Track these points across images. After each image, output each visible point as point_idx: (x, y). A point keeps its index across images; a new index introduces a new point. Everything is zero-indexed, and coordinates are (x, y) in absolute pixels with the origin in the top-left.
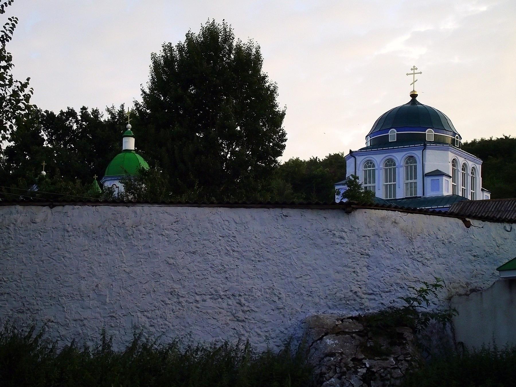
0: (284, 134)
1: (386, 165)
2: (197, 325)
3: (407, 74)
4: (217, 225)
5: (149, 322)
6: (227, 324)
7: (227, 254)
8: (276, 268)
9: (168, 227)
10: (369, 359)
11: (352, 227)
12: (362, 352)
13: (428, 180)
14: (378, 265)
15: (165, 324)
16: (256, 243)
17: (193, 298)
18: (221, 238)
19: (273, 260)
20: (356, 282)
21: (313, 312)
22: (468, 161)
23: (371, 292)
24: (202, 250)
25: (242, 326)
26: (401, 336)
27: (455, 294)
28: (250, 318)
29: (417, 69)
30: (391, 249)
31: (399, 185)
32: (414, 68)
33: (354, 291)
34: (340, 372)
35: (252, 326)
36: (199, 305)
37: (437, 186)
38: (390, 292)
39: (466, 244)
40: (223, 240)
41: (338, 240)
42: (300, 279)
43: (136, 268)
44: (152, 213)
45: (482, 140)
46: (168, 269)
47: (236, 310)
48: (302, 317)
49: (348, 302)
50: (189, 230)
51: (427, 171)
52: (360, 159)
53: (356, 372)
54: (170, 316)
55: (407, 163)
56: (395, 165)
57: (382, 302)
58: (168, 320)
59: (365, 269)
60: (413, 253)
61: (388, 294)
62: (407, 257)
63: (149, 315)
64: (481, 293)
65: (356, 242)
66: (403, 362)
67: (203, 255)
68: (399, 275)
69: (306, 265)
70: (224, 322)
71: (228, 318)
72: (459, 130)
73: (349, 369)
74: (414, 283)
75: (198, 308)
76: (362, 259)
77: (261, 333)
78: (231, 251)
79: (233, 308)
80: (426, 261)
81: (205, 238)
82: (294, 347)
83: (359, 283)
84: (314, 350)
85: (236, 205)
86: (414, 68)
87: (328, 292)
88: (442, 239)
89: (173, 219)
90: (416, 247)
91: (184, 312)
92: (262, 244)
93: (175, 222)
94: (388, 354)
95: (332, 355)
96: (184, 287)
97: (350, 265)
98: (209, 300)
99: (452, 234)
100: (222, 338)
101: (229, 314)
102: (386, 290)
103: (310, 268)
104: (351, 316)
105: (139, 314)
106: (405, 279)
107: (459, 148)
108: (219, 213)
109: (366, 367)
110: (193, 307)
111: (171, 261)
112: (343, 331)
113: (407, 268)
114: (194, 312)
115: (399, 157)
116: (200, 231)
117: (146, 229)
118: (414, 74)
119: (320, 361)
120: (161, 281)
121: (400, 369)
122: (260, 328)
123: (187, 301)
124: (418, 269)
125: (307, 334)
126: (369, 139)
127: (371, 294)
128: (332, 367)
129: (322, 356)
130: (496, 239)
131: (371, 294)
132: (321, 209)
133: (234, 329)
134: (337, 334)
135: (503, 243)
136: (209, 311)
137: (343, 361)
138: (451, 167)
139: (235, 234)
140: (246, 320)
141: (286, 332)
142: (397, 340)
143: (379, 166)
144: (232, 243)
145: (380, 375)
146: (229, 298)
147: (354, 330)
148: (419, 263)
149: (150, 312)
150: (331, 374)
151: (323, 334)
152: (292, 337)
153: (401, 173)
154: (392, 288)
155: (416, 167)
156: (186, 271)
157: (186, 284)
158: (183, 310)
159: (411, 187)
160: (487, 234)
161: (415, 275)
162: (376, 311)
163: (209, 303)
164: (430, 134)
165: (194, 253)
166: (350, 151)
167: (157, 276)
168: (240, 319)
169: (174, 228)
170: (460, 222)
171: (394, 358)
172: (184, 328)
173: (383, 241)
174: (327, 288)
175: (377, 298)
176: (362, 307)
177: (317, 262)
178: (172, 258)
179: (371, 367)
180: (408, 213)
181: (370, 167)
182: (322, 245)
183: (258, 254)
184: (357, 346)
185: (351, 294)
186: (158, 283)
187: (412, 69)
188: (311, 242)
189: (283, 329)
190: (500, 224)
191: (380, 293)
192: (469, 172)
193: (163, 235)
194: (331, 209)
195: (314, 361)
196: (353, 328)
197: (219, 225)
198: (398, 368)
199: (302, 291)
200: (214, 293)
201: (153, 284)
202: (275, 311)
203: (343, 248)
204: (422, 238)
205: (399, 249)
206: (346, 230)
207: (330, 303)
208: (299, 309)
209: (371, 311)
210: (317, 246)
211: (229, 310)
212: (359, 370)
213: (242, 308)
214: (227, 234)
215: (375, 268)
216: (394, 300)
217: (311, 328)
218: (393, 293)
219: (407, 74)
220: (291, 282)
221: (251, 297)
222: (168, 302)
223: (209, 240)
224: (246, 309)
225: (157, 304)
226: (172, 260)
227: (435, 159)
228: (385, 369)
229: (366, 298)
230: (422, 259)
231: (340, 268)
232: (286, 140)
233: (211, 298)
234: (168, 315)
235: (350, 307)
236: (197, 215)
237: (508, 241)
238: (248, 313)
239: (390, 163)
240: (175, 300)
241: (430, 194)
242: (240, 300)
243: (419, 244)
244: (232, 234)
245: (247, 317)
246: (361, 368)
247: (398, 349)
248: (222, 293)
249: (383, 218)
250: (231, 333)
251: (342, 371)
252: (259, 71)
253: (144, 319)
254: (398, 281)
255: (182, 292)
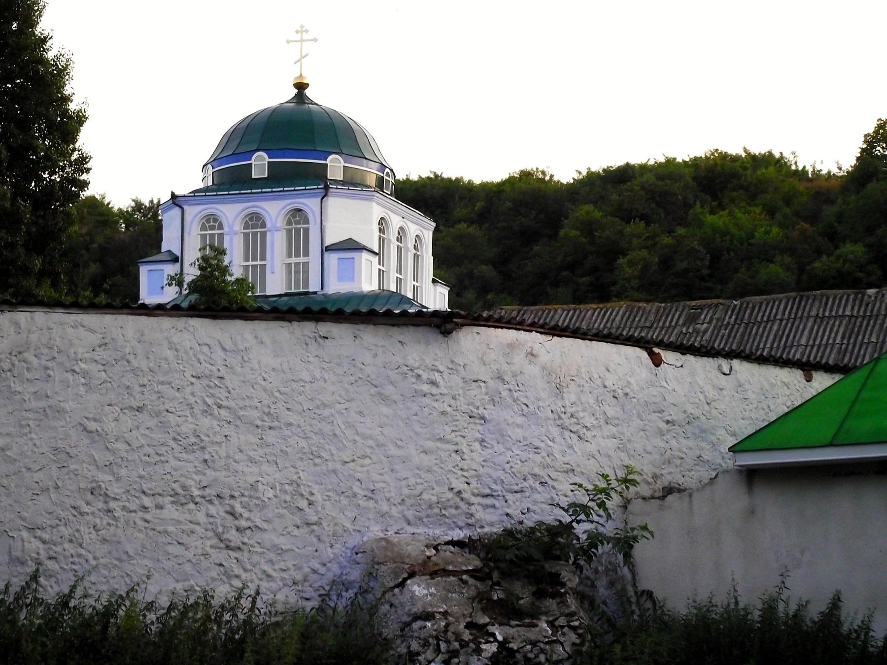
0: (83, 160)
1: (246, 226)
2: (145, 557)
3: (288, 42)
4: (186, 352)
5: (45, 550)
6: (206, 555)
7: (207, 411)
8: (303, 443)
9: (87, 355)
10: (501, 624)
11: (452, 362)
12: (484, 610)
13: (332, 259)
14: (500, 440)
15: (80, 556)
16: (265, 390)
17: (137, 501)
18: (193, 380)
19: (299, 426)
20: (460, 473)
21: (376, 531)
22: (409, 223)
23: (488, 491)
24: (156, 403)
25: (236, 558)
26: (555, 579)
27: (633, 496)
28: (252, 542)
29: (307, 31)
30: (524, 407)
31: (272, 267)
32: (302, 30)
33: (456, 490)
34: (448, 652)
35: (256, 558)
36: (148, 516)
37: (349, 273)
38: (522, 491)
39: (653, 398)
40: (198, 385)
41: (425, 388)
42: (352, 464)
43: (18, 440)
44: (53, 326)
45: (458, 180)
46: (87, 441)
47: (224, 527)
48: (354, 540)
49: (443, 512)
50: (128, 362)
51: (328, 241)
52: (192, 212)
53: (478, 651)
54: (88, 536)
55: (289, 223)
56: (264, 225)
57: (509, 511)
58: (84, 545)
59: (477, 446)
60: (563, 416)
61: (519, 495)
62: (552, 423)
63: (46, 536)
64: (690, 495)
65: (461, 392)
66: (566, 630)
67: (158, 414)
68: (538, 458)
69: (365, 437)
70: (200, 551)
71: (209, 543)
72: (390, 162)
73: (464, 644)
74: (564, 474)
75: (147, 521)
76: (472, 426)
77: (274, 574)
78: (215, 407)
79: (219, 521)
80: (585, 430)
81: (161, 379)
82: (342, 603)
83: (465, 474)
84: (387, 607)
85: (228, 313)
86: (302, 30)
87: (406, 491)
88: (613, 388)
89: (95, 339)
90: (568, 404)
91: (119, 532)
92: (277, 394)
93: (100, 346)
94: (534, 614)
95: (428, 616)
96: (118, 479)
97: (448, 437)
98: (170, 506)
99: (629, 379)
100: (198, 583)
101: (210, 534)
102: (516, 488)
103: (371, 443)
104: (450, 538)
105: (25, 534)
106: (548, 466)
107: (391, 195)
108: (191, 329)
109: (496, 640)
110: (138, 521)
111: (92, 426)
112: (444, 570)
113: (550, 443)
114: (140, 531)
115: (274, 210)
116: (151, 365)
117: (39, 358)
118: (302, 41)
119: (402, 630)
120: (72, 467)
121: (562, 644)
122: (271, 562)
123: (124, 508)
124: (571, 447)
125: (370, 575)
126: (211, 171)
127: (487, 496)
128: (431, 640)
129: (406, 619)
130: (706, 389)
131: (487, 496)
132: (393, 325)
133: (221, 565)
134: (433, 574)
135: (717, 397)
136: (171, 529)
137: (452, 629)
138: (377, 234)
139: (223, 372)
140: (244, 547)
141: (322, 570)
142: (548, 586)
143: (231, 227)
144: (215, 391)
145: (525, 657)
146: (210, 502)
147: (464, 568)
148: (572, 435)
149: (48, 529)
150: (429, 654)
151: (405, 575)
152: (334, 581)
153: (277, 242)
154: (526, 484)
155: (306, 231)
156: (121, 446)
157: (123, 472)
158: (117, 527)
159: (297, 272)
160: (689, 380)
161: (566, 460)
162: (495, 530)
163: (171, 512)
164: (335, 165)
165: (139, 409)
166: (173, 194)
167: (63, 456)
168: (232, 544)
169: (97, 358)
170: (644, 354)
171: (548, 622)
172: (117, 563)
173: (510, 390)
174: (404, 483)
175: (497, 504)
176: (470, 521)
177: (386, 431)
178: (95, 420)
179: (506, 641)
180: (554, 335)
181: (212, 228)
182: (395, 397)
183: (269, 414)
184: (473, 599)
185: (450, 495)
186: (66, 470)
187: (297, 32)
188: (373, 390)
189: (317, 566)
190: (711, 359)
191: (505, 493)
192: (410, 244)
193: (74, 371)
194: (414, 325)
195: (390, 630)
196: (462, 564)
197: (191, 353)
198: (557, 641)
199: (356, 489)
200: (180, 491)
201: (55, 472)
202: (301, 530)
203: (435, 404)
204: (579, 386)
205: (539, 408)
206: (441, 368)
207: (410, 514)
208: (348, 525)
209: (487, 529)
210: (384, 398)
211: (210, 527)
212: (484, 646)
213: (237, 523)
214: (207, 372)
215: (495, 443)
216: (539, 509)
217: (379, 563)
218: (527, 494)
219: (288, 42)
220: (334, 471)
221: (255, 501)
222: (86, 509)
223: (170, 384)
224: (244, 523)
225: (63, 514)
226: (93, 423)
227: (348, 216)
228: (534, 644)
229: (479, 504)
230: (578, 427)
231: (430, 444)
232: (88, 170)
233: (173, 503)
234: (86, 536)
235: (447, 520)
236: (146, 332)
237: (725, 392)
238: (248, 532)
239: (255, 221)
240: (101, 505)
241: (335, 287)
242: (232, 507)
243: (573, 398)
244: (216, 372)
245: (246, 540)
246: (487, 642)
247: (551, 604)
248: (196, 493)
249: (511, 346)
250: (214, 574)
251: (451, 648)
252: (34, 24)
253: (36, 544)
254: (537, 470)
255: (115, 489)
